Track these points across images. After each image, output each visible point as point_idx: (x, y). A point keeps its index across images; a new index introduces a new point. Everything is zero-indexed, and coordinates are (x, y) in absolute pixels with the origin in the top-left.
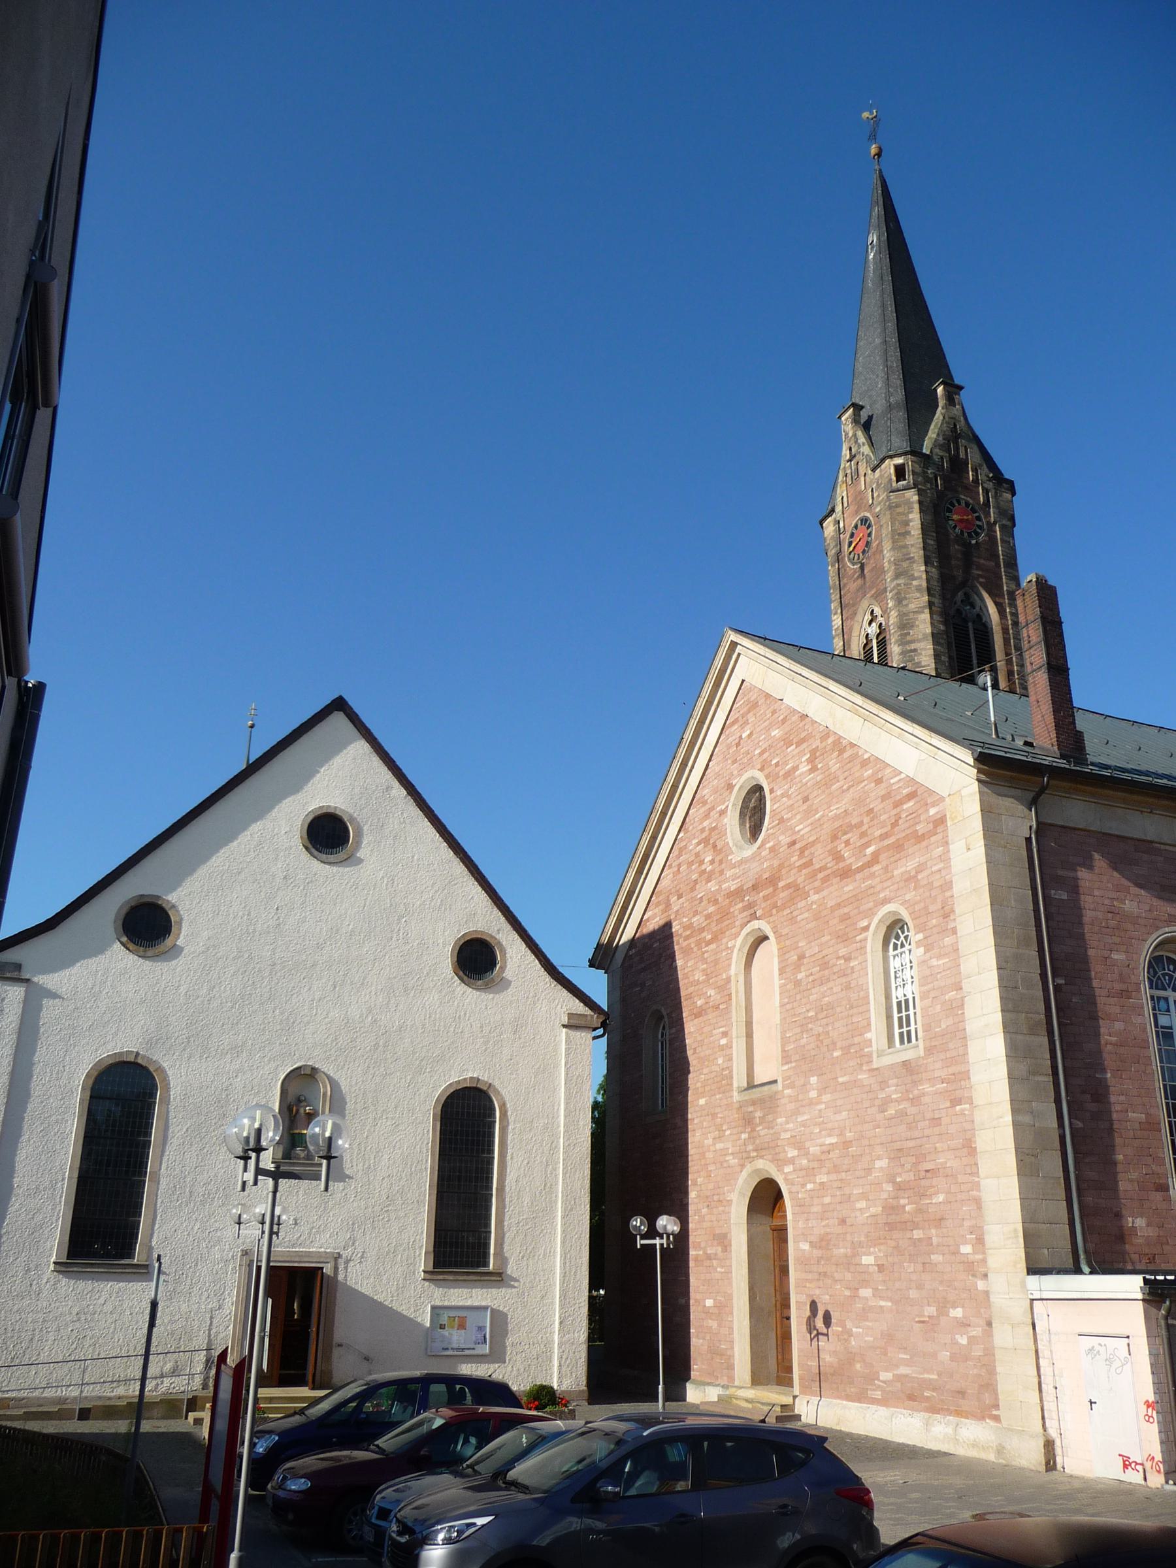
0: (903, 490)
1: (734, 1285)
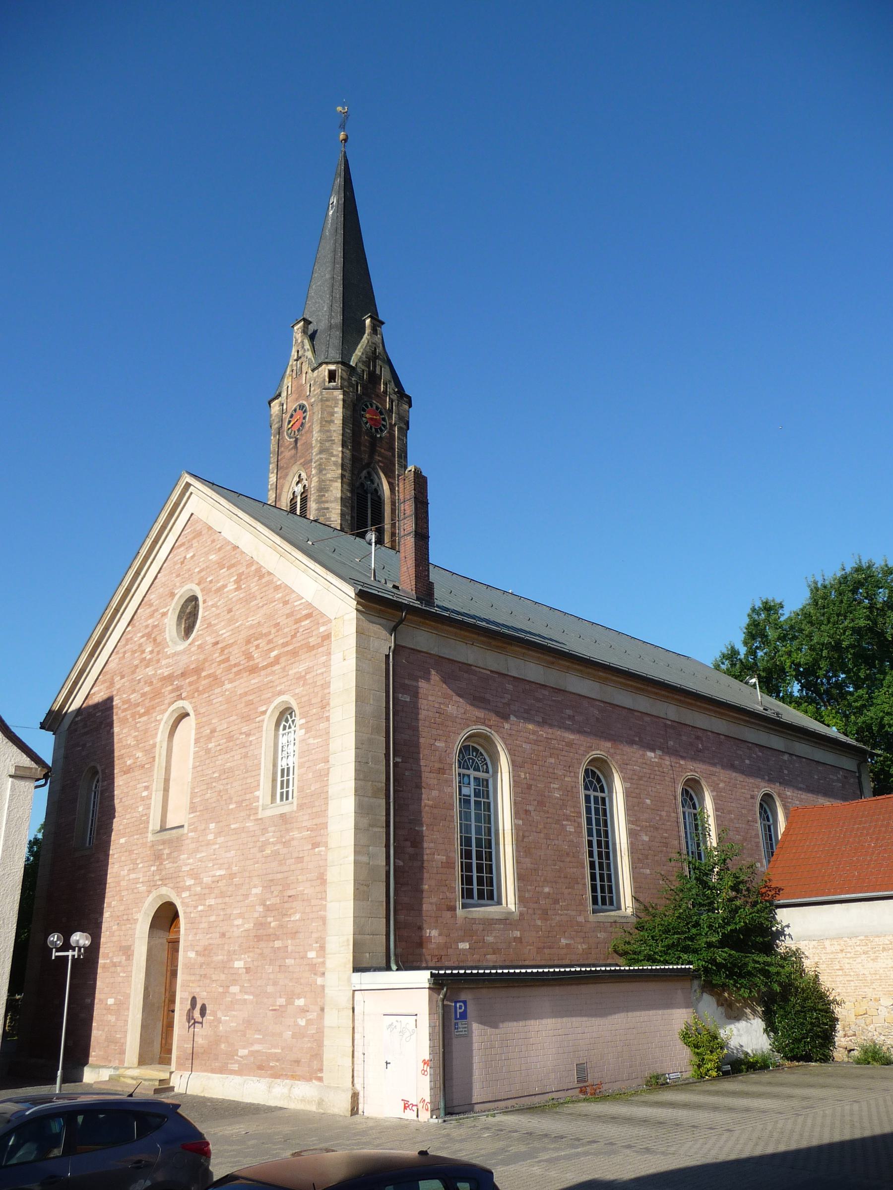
0: (332, 389)
1: (133, 987)
